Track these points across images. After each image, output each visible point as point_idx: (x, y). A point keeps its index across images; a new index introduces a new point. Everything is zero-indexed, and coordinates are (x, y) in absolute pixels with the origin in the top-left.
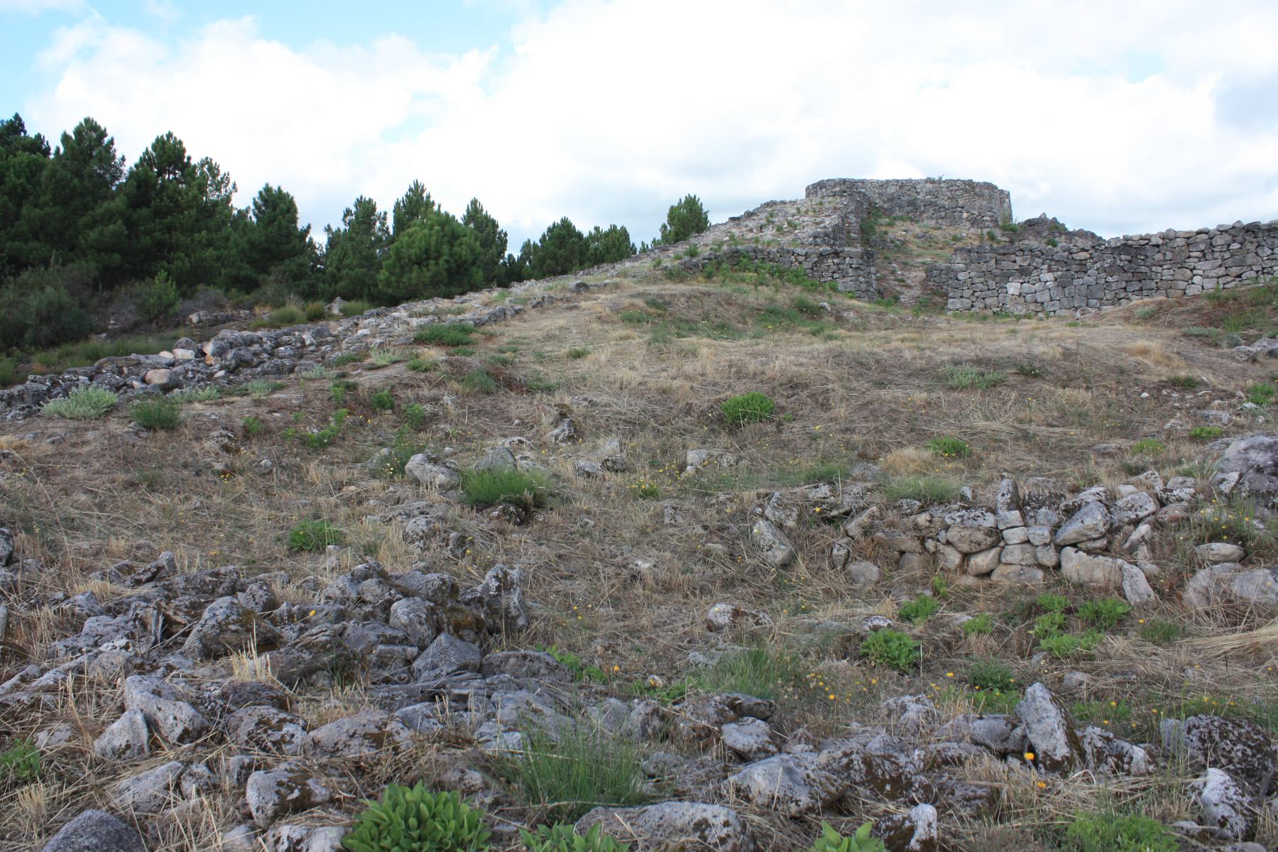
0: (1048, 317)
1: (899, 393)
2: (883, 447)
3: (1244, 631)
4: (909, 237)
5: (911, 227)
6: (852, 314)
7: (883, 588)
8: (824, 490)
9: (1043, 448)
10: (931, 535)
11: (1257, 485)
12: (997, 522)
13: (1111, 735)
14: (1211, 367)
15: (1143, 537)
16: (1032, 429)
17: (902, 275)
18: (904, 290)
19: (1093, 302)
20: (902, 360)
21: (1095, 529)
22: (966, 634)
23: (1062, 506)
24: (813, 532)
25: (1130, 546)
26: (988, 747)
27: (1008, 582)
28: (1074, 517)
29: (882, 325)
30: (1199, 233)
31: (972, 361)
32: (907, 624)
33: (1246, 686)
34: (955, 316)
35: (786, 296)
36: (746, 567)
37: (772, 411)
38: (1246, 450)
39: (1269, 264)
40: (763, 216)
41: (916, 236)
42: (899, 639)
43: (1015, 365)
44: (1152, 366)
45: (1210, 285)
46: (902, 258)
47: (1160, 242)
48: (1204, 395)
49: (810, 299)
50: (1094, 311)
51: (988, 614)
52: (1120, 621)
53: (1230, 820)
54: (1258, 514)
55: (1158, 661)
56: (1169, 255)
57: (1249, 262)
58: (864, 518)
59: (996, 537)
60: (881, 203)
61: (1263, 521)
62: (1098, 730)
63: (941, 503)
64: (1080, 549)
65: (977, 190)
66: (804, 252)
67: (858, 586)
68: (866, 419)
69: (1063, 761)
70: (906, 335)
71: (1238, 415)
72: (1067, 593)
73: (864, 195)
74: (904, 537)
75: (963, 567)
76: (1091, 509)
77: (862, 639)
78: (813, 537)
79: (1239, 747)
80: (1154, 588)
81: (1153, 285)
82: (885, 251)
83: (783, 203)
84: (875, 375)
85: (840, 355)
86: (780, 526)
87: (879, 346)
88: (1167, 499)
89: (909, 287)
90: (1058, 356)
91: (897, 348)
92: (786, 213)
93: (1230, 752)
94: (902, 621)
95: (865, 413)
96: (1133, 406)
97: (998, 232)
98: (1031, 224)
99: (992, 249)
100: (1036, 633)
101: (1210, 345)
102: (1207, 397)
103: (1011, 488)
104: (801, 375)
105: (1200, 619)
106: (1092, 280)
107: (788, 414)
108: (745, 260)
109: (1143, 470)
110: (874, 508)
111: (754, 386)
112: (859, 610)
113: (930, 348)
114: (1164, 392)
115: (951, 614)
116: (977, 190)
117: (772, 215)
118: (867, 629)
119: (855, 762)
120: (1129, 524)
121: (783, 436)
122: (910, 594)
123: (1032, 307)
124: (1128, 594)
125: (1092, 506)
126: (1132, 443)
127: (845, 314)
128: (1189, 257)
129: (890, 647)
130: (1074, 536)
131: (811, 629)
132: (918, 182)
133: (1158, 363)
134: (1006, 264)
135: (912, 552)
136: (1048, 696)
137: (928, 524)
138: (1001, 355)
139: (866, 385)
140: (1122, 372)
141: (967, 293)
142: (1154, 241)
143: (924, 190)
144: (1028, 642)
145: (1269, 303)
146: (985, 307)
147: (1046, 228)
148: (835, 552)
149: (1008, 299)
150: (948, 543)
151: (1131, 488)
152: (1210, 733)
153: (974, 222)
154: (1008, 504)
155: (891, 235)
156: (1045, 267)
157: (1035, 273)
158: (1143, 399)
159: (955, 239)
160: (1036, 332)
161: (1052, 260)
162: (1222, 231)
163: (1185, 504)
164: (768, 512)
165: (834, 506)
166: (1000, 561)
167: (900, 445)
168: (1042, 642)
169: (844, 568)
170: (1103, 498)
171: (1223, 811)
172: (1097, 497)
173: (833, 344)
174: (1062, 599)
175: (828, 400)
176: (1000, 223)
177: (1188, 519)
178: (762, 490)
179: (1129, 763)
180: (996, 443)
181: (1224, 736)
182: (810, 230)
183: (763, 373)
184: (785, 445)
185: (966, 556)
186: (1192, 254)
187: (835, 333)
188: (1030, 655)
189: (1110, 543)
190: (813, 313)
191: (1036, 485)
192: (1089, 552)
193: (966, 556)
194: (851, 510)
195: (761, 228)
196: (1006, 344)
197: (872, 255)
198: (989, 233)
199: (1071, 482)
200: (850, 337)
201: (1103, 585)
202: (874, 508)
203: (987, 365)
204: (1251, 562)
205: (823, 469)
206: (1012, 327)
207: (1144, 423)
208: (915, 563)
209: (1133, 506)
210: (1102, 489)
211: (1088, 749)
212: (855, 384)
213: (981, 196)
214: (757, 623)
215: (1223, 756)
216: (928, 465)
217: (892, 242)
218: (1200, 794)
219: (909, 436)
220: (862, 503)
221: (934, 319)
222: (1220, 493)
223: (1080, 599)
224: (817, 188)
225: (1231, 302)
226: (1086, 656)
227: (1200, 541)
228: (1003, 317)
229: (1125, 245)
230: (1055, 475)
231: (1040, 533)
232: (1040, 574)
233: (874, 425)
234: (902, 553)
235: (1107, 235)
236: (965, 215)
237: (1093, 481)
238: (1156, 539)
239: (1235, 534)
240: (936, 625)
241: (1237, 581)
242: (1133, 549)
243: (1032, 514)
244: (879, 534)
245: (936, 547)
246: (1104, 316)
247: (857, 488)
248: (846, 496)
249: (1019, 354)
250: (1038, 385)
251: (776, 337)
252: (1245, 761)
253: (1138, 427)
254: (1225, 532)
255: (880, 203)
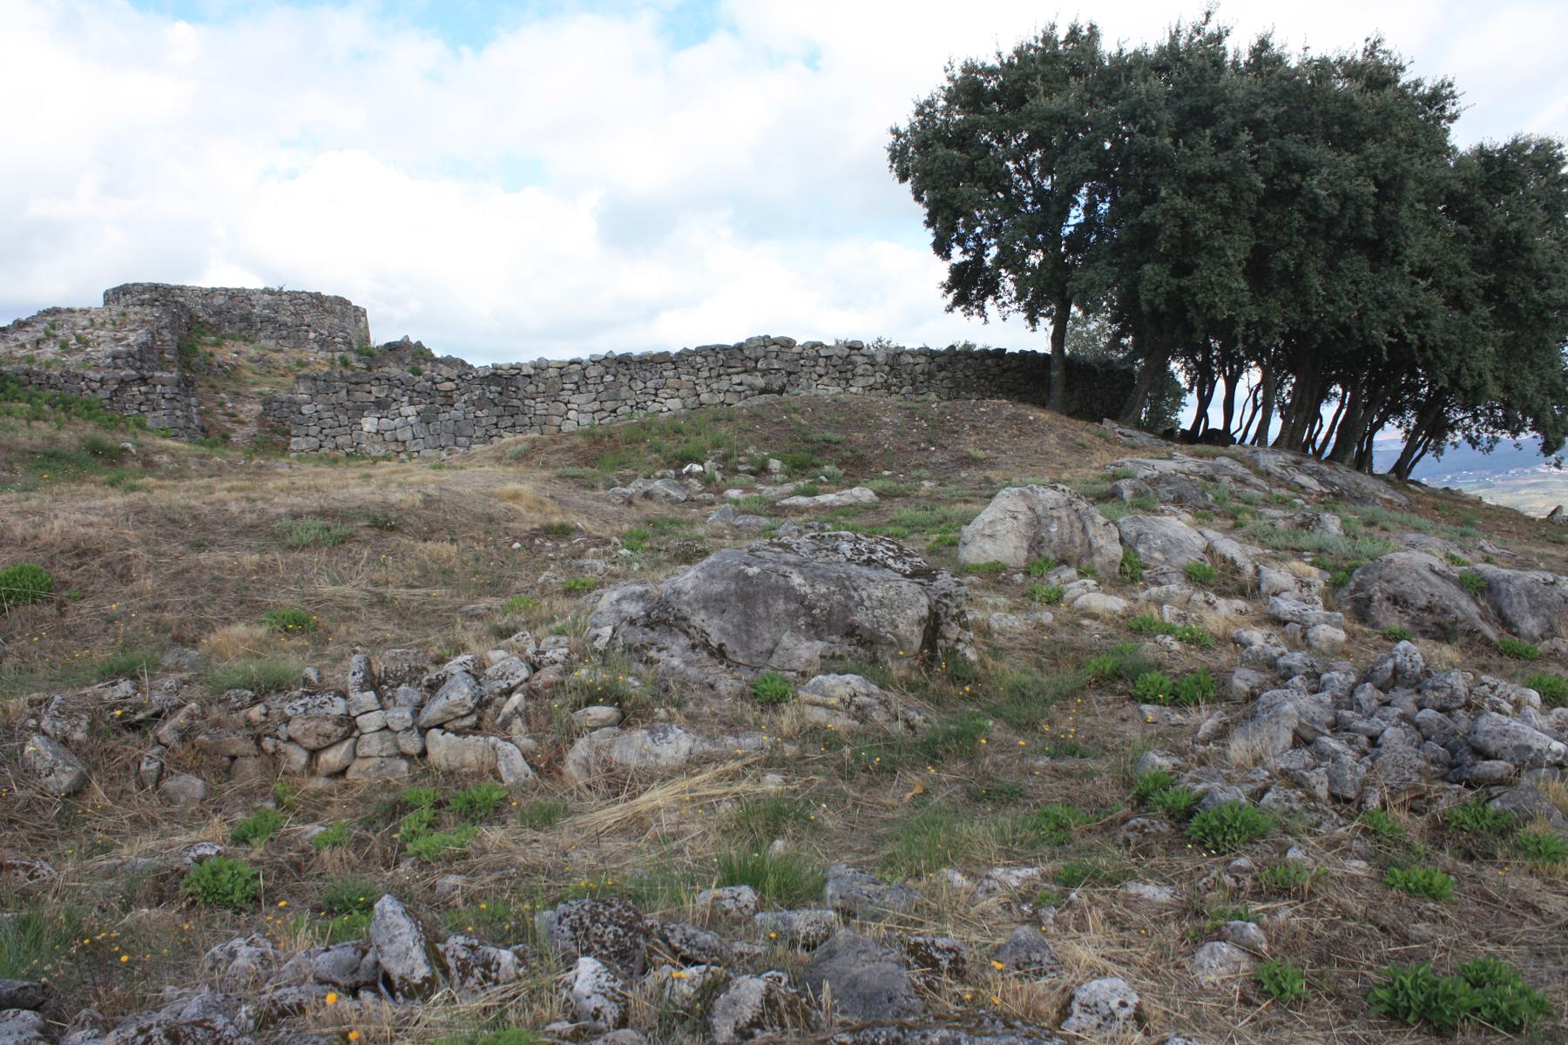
0: (411, 458)
1: (223, 556)
2: (205, 626)
3: (626, 801)
4: (243, 361)
5: (244, 348)
6: (165, 458)
7: (212, 804)
8: (125, 687)
9: (403, 614)
10: (268, 731)
11: (630, 639)
12: (348, 707)
13: (476, 942)
14: (585, 511)
15: (516, 708)
16: (390, 591)
17: (233, 407)
18: (236, 426)
19: (462, 440)
20: (228, 515)
21: (462, 704)
22: (318, 849)
23: (424, 681)
24: (111, 743)
25: (503, 721)
26: (335, 984)
27: (366, 780)
28: (439, 693)
29: (206, 471)
30: (572, 363)
31: (315, 513)
32: (245, 848)
33: (629, 861)
34: (299, 458)
35: (70, 436)
36: (15, 803)
37: (50, 587)
38: (618, 601)
39: (642, 398)
40: (40, 327)
41: (251, 360)
42: (231, 868)
43: (367, 516)
44: (524, 513)
45: (585, 420)
46: (232, 386)
47: (532, 372)
48: (578, 543)
49: (107, 438)
50: (461, 450)
51: (344, 821)
52: (497, 809)
53: (603, 1010)
54: (634, 671)
55: (538, 849)
56: (542, 387)
57: (623, 395)
58: (180, 719)
59: (349, 726)
60: (206, 317)
61: (638, 676)
62: (461, 939)
63: (279, 691)
64: (447, 730)
65: (327, 305)
66: (98, 377)
67: (176, 808)
68: (181, 592)
69: (423, 985)
70: (235, 483)
71: (614, 563)
72: (436, 783)
73: (183, 305)
74: (234, 738)
75: (311, 768)
76: (457, 682)
77: (182, 875)
78: (112, 750)
79: (611, 928)
80: (532, 766)
81: (527, 420)
82: (211, 378)
83: (71, 311)
84: (192, 535)
85: (144, 511)
86: (65, 741)
87: (196, 498)
88: (540, 662)
89: (242, 423)
90: (418, 503)
91: (220, 500)
92: (75, 325)
93: (602, 936)
94: (237, 845)
95: (180, 584)
96: (504, 559)
97: (352, 357)
98: (391, 348)
99: (342, 378)
100: (402, 836)
101: (586, 487)
102: (582, 545)
103: (363, 665)
104: (90, 538)
105: (582, 794)
106: (459, 414)
107: (74, 592)
108: (14, 387)
109: (515, 631)
110: (194, 705)
111: (23, 555)
112: (177, 839)
113: (262, 499)
114: (537, 541)
115: (300, 827)
116: (327, 305)
117: (53, 327)
118: (189, 860)
119: (155, 1038)
120: (500, 695)
121: (68, 621)
122: (247, 808)
123: (393, 446)
124: (504, 776)
125: (457, 677)
126: (503, 601)
127: (156, 458)
128: (563, 390)
129: (220, 880)
130: (439, 715)
131: (111, 873)
132: (254, 292)
133: (530, 508)
134: (360, 396)
135: (246, 756)
136: (399, 909)
137: (263, 718)
138: (353, 505)
139: (181, 548)
140: (491, 520)
141: (314, 430)
142: (525, 372)
143: (261, 302)
144: (393, 849)
145: (644, 440)
146: (337, 447)
147: (408, 353)
148: (144, 767)
149: (364, 438)
150: (290, 740)
151: (501, 653)
152: (581, 919)
153: (323, 344)
154: (360, 684)
155: (219, 358)
156: (406, 399)
157: (394, 406)
158: (514, 550)
159: (300, 364)
160: (393, 477)
161: (414, 391)
162: (595, 362)
163: (559, 666)
164: (46, 724)
165: (140, 707)
166: (355, 755)
167: (227, 622)
168: (409, 846)
169: (157, 786)
170: (471, 668)
171: (596, 1002)
172: (463, 668)
173: (134, 497)
174: (431, 791)
175: (129, 570)
176: (356, 347)
177: (563, 683)
178: (35, 695)
179: (497, 971)
180: (348, 612)
181: (594, 921)
182: (108, 348)
183: (36, 537)
184: (70, 632)
185: (314, 753)
186: (566, 386)
187: (139, 482)
188: (397, 864)
189: (480, 719)
190: (112, 457)
191: (394, 659)
192: (457, 732)
193: (314, 753)
194: (163, 711)
195: (38, 342)
196: (357, 491)
197: (192, 383)
198: (341, 358)
199: (435, 651)
200: (161, 487)
201: (476, 769)
202: (194, 705)
203: (334, 517)
204: (629, 724)
205: (122, 659)
206: (366, 471)
207: (516, 578)
208: (250, 768)
209: (504, 674)
210: (469, 657)
211: (451, 963)
212: (165, 547)
213: (332, 312)
214: (31, 877)
215: (595, 942)
216: (264, 643)
217: (220, 366)
218: (572, 989)
219: (238, 609)
220: (176, 700)
221: (272, 462)
222: (595, 651)
223: (452, 789)
224: (116, 295)
225: (606, 439)
226: (460, 854)
227: (577, 706)
228: (357, 459)
229: (494, 374)
230: (417, 646)
231: (400, 716)
232: (403, 765)
233: (192, 598)
234: (233, 758)
235: (479, 361)
236: (312, 335)
237: (460, 648)
238: (531, 710)
239: (612, 696)
240: (280, 844)
241: (616, 747)
242: (506, 724)
243: (390, 694)
244: (202, 737)
245: (276, 746)
246: (472, 457)
247: (169, 682)
248: (155, 693)
249: (372, 502)
250: (395, 539)
251: (56, 489)
252: (617, 942)
253: (509, 583)
254: (600, 694)
255: (203, 316)
